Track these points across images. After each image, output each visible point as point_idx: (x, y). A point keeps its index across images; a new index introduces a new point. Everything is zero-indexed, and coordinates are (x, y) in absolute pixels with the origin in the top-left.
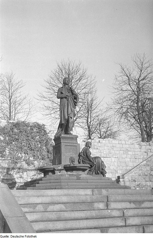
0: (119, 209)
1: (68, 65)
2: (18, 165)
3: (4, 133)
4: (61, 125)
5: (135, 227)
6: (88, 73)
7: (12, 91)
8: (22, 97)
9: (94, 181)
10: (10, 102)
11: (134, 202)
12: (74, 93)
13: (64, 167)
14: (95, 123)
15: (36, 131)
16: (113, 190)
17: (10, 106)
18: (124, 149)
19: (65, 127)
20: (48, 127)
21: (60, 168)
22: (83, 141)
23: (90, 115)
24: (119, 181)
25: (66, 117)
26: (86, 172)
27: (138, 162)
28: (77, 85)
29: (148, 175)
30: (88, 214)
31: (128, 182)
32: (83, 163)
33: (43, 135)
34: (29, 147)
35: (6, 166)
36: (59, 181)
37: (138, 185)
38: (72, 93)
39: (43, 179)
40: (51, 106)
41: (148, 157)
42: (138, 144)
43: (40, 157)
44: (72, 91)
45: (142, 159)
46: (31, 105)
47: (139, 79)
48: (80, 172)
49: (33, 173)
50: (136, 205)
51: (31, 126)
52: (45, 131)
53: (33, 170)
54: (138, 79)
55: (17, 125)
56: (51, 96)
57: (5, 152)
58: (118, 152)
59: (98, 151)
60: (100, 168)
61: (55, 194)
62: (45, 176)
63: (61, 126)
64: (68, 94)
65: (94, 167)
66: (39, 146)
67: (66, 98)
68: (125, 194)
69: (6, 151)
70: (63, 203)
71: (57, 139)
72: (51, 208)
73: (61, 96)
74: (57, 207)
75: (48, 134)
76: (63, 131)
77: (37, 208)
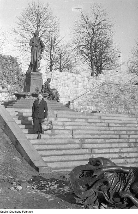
0: (62, 122)
1: (37, 5)
4: (31, 65)
5: (68, 130)
6: (54, 15)
13: (32, 94)
14: (56, 56)
15: (10, 62)
18: (76, 81)
20: (19, 59)
21: (29, 95)
22: (46, 72)
23: (52, 50)
24: (70, 104)
25: (35, 60)
27: (85, 91)
28: (44, 24)
29: (91, 101)
32: (45, 93)
33: (15, 66)
34: (4, 74)
37: (83, 108)
38: (40, 43)
39: (17, 101)
40: (21, 40)
41: (94, 88)
42: (87, 77)
44: (40, 41)
46: (4, 37)
47: (94, 24)
49: (6, 94)
51: (6, 59)
52: (17, 63)
53: (6, 92)
54: (93, 24)
56: (22, 31)
58: (71, 83)
61: (28, 112)
62: (19, 99)
63: (31, 66)
64: (38, 44)
65: (51, 95)
66: (12, 74)
67: (36, 46)
68: (67, 114)
71: (28, 75)
73: (32, 44)
75: (19, 66)
76: (32, 69)
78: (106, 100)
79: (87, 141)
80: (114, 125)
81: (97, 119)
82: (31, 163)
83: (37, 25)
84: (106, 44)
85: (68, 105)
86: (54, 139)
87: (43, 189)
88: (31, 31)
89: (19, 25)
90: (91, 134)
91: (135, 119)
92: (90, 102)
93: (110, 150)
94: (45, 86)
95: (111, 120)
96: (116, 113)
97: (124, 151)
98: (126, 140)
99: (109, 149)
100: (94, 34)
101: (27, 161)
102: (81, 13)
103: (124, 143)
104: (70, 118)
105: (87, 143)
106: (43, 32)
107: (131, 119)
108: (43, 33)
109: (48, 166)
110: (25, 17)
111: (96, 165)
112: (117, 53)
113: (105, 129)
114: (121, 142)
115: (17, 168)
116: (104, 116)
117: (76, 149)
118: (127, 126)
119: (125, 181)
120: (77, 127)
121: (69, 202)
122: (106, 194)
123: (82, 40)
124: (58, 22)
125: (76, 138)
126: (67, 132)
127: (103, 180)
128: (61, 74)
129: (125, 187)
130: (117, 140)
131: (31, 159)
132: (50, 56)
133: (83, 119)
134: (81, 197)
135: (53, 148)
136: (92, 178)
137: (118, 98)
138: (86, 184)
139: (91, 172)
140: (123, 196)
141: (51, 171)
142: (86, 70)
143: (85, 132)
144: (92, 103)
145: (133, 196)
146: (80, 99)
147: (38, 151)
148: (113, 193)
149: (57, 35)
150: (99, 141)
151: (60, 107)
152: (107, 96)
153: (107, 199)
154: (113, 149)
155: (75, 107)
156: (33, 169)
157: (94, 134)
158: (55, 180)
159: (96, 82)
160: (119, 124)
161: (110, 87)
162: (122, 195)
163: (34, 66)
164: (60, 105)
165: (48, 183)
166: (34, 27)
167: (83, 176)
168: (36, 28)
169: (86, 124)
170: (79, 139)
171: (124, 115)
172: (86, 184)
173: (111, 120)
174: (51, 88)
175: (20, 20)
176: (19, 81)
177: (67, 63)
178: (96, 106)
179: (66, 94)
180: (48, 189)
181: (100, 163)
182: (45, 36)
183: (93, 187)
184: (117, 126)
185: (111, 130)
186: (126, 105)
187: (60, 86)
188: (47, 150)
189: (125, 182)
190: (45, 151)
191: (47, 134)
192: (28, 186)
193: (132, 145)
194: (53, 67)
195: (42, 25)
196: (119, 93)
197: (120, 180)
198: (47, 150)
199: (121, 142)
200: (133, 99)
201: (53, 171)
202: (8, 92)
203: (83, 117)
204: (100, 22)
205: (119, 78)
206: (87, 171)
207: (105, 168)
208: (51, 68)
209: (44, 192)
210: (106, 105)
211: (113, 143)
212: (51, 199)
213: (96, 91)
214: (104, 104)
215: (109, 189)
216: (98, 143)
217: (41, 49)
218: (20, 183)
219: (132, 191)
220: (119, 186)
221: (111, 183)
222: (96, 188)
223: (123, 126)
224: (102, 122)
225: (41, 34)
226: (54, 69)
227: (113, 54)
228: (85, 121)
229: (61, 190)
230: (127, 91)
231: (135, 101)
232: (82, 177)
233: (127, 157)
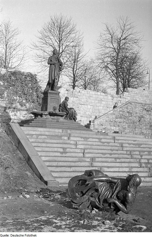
0: (74, 141)
1: (60, 18)
2: (14, 106)
3: (4, 80)
4: (49, 84)
6: (77, 28)
7: (9, 37)
8: (17, 44)
9: (68, 124)
10: (6, 47)
11: (84, 138)
12: (60, 61)
13: (49, 113)
14: (79, 72)
17: (6, 51)
18: (98, 99)
19: (52, 85)
21: (46, 113)
23: (75, 66)
26: (63, 117)
30: (58, 141)
32: (62, 112)
33: (34, 84)
34: (23, 92)
35: (4, 105)
36: (45, 122)
37: (104, 128)
42: (111, 95)
43: (31, 100)
47: (120, 39)
49: (25, 112)
50: (84, 140)
51: (25, 76)
52: (36, 80)
53: (25, 110)
55: (14, 74)
56: (43, 45)
57: (3, 95)
58: (93, 101)
59: (78, 99)
62: (36, 118)
64: (56, 62)
65: (69, 115)
66: (31, 91)
67: (54, 64)
69: (5, 94)
70: (46, 135)
71: (46, 93)
72: (40, 137)
76: (50, 88)
77: (33, 136)
79: (97, 159)
80: (127, 145)
81: (111, 139)
82: (41, 178)
83: (60, 39)
84: (134, 60)
85: (88, 126)
86: (65, 157)
87: (48, 198)
88: (53, 45)
89: (40, 39)
90: (102, 154)
94: (63, 106)
95: (125, 140)
96: (140, 134)
98: (138, 160)
100: (120, 49)
101: (38, 175)
102: (107, 26)
103: (136, 163)
105: (97, 162)
106: (66, 47)
107: (147, 140)
108: (65, 48)
110: (47, 31)
112: (145, 69)
115: (27, 181)
116: (119, 136)
117: (86, 167)
118: (142, 146)
120: (90, 147)
121: (68, 208)
122: (97, 200)
123: (107, 55)
124: (81, 37)
125: (87, 156)
126: (79, 151)
127: (94, 188)
128: (84, 92)
129: (113, 194)
132: (73, 72)
133: (96, 138)
136: (86, 186)
137: (143, 119)
138: (81, 191)
139: (85, 181)
141: (58, 186)
142: (111, 87)
143: (96, 151)
144: (115, 123)
147: (48, 167)
148: (103, 199)
149: (81, 49)
150: (110, 160)
151: (78, 126)
152: (130, 116)
153: (97, 204)
155: (96, 127)
156: (42, 183)
157: (105, 154)
159: (121, 101)
160: (134, 144)
161: (135, 106)
162: (109, 200)
163: (52, 84)
166: (56, 41)
167: (79, 184)
168: (59, 42)
169: (99, 143)
170: (90, 158)
171: (139, 136)
173: (125, 140)
174: (69, 107)
175: (41, 34)
176: (39, 99)
177: (93, 80)
178: (119, 126)
179: (87, 113)
180: (52, 198)
181: (93, 174)
182: (68, 51)
183: (86, 194)
184: (132, 146)
185: (123, 150)
187: (81, 105)
188: (57, 166)
192: (35, 196)
194: (76, 84)
195: (64, 39)
196: (144, 113)
197: (109, 188)
198: (57, 166)
201: (60, 185)
202: (27, 110)
203: (97, 137)
204: (127, 37)
205: (146, 97)
207: (96, 178)
208: (74, 84)
209: (48, 200)
210: (130, 126)
211: (124, 162)
212: (52, 205)
213: (119, 110)
214: (127, 125)
217: (60, 67)
218: (28, 193)
220: (108, 194)
221: (101, 190)
222: (88, 195)
223: (137, 146)
225: (63, 49)
226: (77, 86)
227: (141, 71)
228: (98, 141)
229: (64, 199)
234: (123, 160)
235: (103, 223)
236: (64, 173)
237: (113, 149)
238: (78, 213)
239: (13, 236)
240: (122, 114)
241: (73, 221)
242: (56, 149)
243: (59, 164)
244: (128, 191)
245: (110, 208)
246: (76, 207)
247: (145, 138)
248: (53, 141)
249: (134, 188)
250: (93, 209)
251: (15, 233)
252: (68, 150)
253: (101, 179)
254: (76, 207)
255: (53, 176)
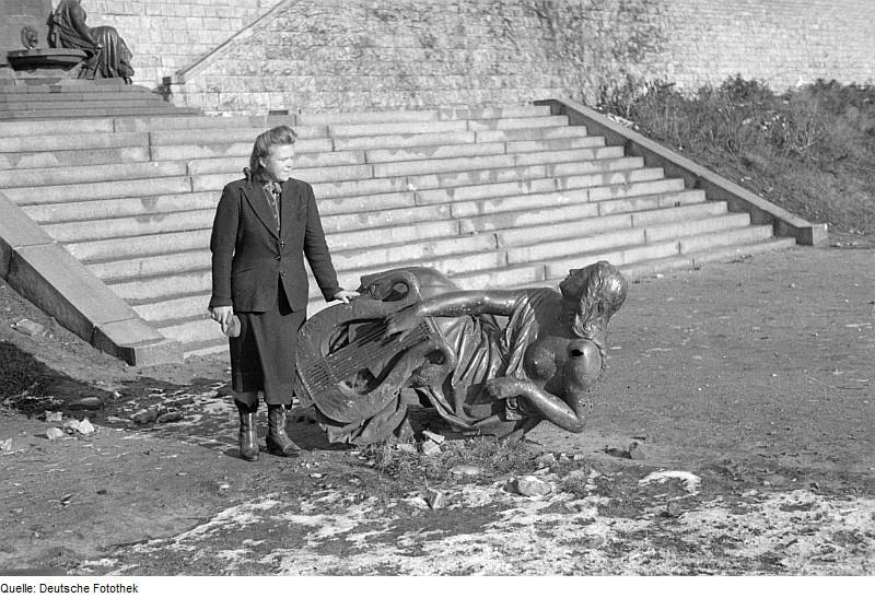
0: (177, 162)
13: (9, 59)
16: (161, 119)
24: (169, 92)
26: (74, 71)
30: (110, 171)
31: (197, 95)
32: (65, 47)
37: (227, 104)
41: (261, 13)
45: (240, 21)
48: (57, 73)
60: (116, 58)
65: (96, 57)
72: (25, 160)
74: (39, 159)
78: (320, 62)
80: (385, 156)
81: (314, 138)
86: (161, 233)
87: (177, 419)
91: (463, 124)
92: (254, 73)
93: (387, 255)
96: (367, 109)
97: (443, 254)
99: (385, 251)
103: (437, 220)
104: (208, 145)
109: (164, 339)
111: (394, 296)
113: (354, 173)
114: (424, 218)
116: (341, 124)
118: (437, 154)
119: (505, 339)
127: (424, 348)
129: (506, 361)
130: (410, 213)
131: (90, 319)
134: (348, 421)
135: (165, 270)
136: (383, 345)
138: (359, 373)
140: (502, 392)
145: (539, 389)
146: (213, 65)
152: (322, 43)
153: (443, 413)
154: (398, 248)
156: (106, 356)
158: (211, 384)
162: (499, 389)
164: (139, 95)
165: (189, 396)
167: (346, 342)
172: (359, 373)
178: (282, 89)
180: (198, 417)
183: (390, 376)
184: (401, 159)
186: (402, 76)
188: (140, 278)
189: (503, 344)
190: (134, 283)
191: (128, 216)
192: (114, 418)
193: (470, 226)
196: (370, 29)
198: (140, 278)
199: (425, 221)
200: (431, 47)
201: (186, 355)
206: (359, 325)
207: (429, 301)
213: (275, 25)
214: (313, 81)
215: (451, 375)
216: (336, 233)
219: (533, 373)
220: (486, 364)
224: (337, 149)
230: (405, 18)
231: (438, 57)
232: (342, 346)
233: (457, 271)
234: (389, 217)
235: (514, 488)
236: (180, 304)
237: (336, 177)
238: (363, 465)
239: (50, 589)
240: (290, 40)
241: (376, 505)
242: (112, 207)
243: (145, 265)
244: (579, 337)
245: (504, 420)
246: (344, 441)
247: (440, 120)
248: (89, 173)
249: (601, 322)
250: (420, 438)
251: (55, 581)
252: (162, 203)
253: (451, 306)
254: (344, 441)
255: (143, 320)
